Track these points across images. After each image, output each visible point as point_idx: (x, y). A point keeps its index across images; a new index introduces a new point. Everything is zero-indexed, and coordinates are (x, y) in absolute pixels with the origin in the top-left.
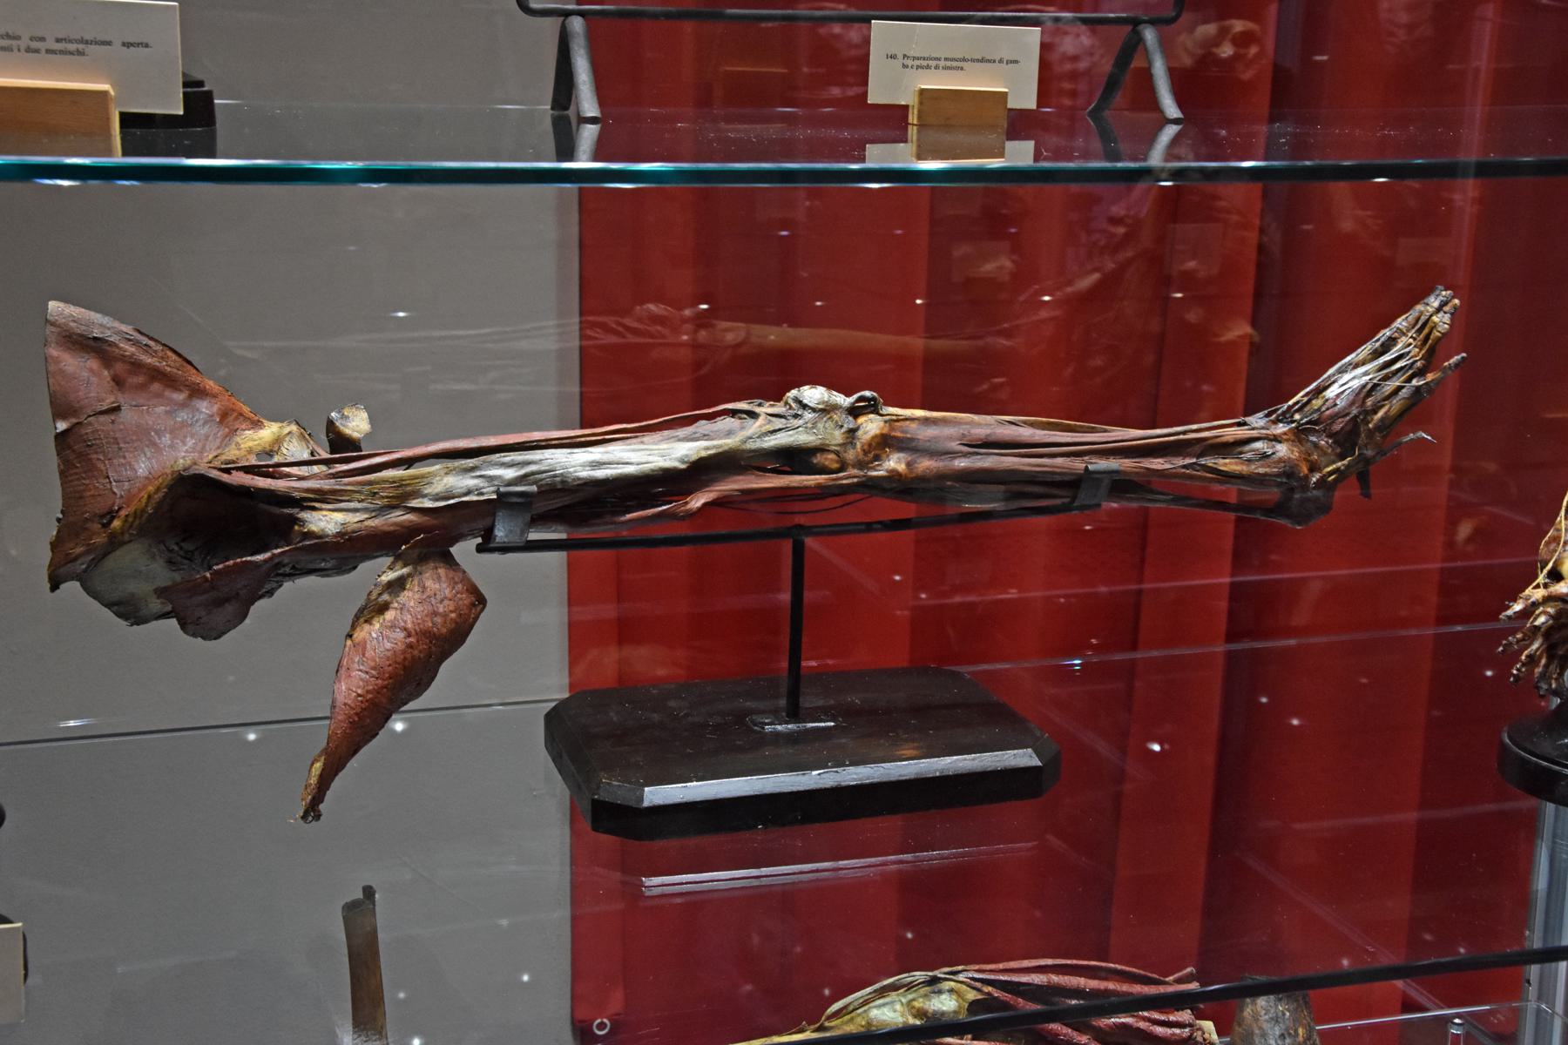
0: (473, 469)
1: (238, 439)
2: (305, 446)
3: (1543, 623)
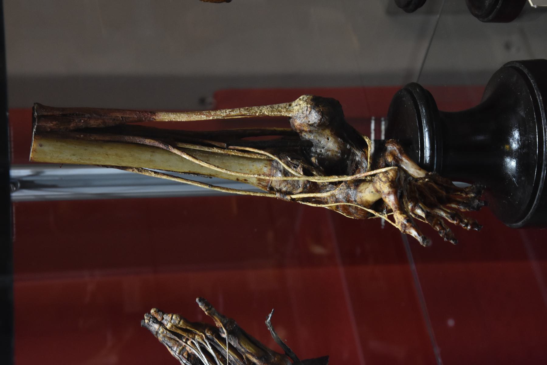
3: (423, 210)
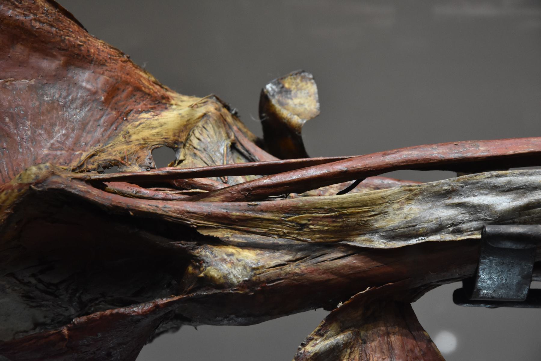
0: (448, 194)
1: (129, 127)
2: (224, 135)
